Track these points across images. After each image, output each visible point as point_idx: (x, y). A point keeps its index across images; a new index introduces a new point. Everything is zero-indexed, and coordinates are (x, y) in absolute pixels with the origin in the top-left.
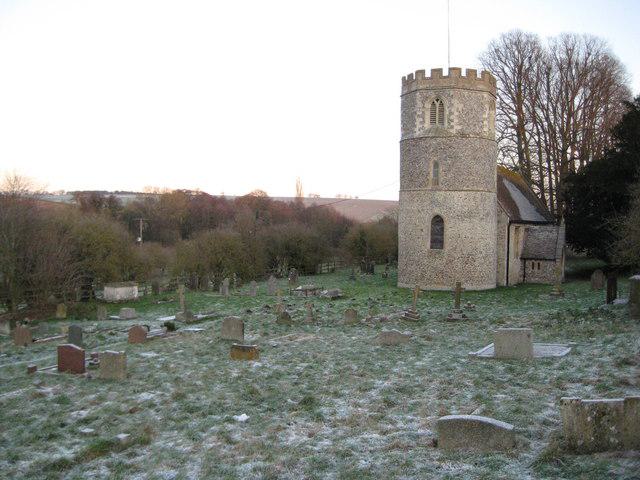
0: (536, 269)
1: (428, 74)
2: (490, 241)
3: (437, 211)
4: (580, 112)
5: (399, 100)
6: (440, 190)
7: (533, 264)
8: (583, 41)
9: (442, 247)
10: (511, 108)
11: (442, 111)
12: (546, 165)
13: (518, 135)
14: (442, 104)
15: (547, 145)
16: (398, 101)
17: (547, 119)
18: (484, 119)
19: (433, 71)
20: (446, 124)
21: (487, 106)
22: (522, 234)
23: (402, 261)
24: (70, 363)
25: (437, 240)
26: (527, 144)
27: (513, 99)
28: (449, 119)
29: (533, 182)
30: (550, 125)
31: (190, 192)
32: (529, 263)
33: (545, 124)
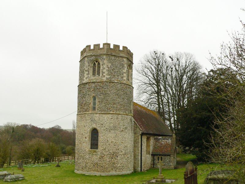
0: (160, 161)
1: (92, 48)
2: (130, 144)
3: (94, 126)
4: (185, 85)
5: (79, 64)
6: (96, 114)
7: (158, 157)
11: (99, 67)
14: (99, 64)
16: (78, 65)
18: (124, 72)
19: (95, 46)
20: (101, 75)
25: (94, 144)
26: (162, 101)
28: (102, 72)
30: (173, 93)
31: (27, 125)
32: (156, 157)
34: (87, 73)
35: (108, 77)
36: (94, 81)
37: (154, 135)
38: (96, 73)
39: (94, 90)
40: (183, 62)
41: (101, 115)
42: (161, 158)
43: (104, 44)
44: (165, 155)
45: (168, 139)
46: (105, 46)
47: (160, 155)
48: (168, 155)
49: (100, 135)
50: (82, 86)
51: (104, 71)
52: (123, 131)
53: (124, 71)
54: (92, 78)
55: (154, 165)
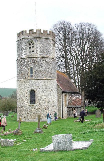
1: (28, 32)
3: (32, 88)
7: (72, 109)
8: (87, 24)
9: (35, 103)
10: (62, 50)
11: (33, 47)
12: (76, 72)
13: (65, 60)
14: (33, 44)
15: (76, 64)
17: (76, 55)
19: (30, 31)
20: (35, 52)
21: (52, 45)
22: (67, 97)
23: (18, 109)
24: (50, 115)
25: (33, 100)
26: (68, 63)
27: (63, 46)
29: (71, 78)
33: (75, 56)
34: (25, 50)
35: (41, 54)
36: (31, 56)
37: (69, 93)
38: (32, 51)
39: (31, 63)
40: (86, 30)
41: (37, 80)
42: (75, 109)
43: (37, 30)
44: (77, 107)
45: (79, 96)
46: (38, 32)
47: (73, 107)
48: (79, 107)
49: (37, 94)
50: (20, 61)
51: (38, 49)
52: (51, 91)
53: (51, 49)
54: (29, 54)
55: (69, 114)
